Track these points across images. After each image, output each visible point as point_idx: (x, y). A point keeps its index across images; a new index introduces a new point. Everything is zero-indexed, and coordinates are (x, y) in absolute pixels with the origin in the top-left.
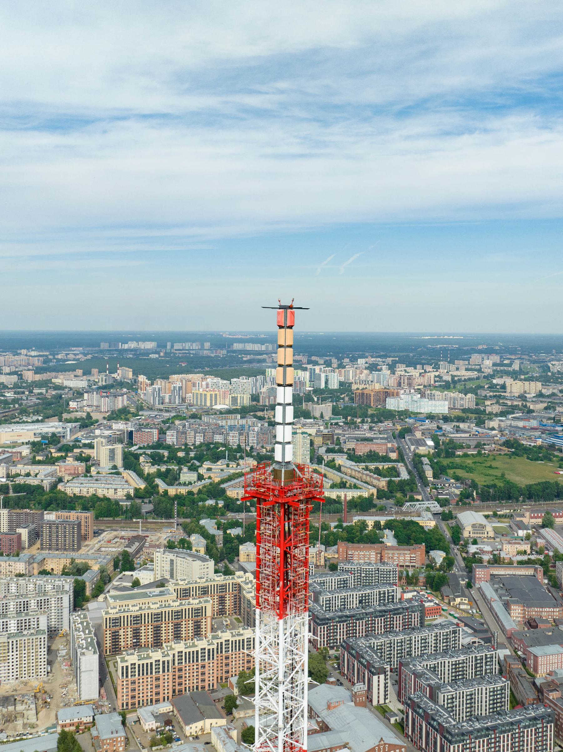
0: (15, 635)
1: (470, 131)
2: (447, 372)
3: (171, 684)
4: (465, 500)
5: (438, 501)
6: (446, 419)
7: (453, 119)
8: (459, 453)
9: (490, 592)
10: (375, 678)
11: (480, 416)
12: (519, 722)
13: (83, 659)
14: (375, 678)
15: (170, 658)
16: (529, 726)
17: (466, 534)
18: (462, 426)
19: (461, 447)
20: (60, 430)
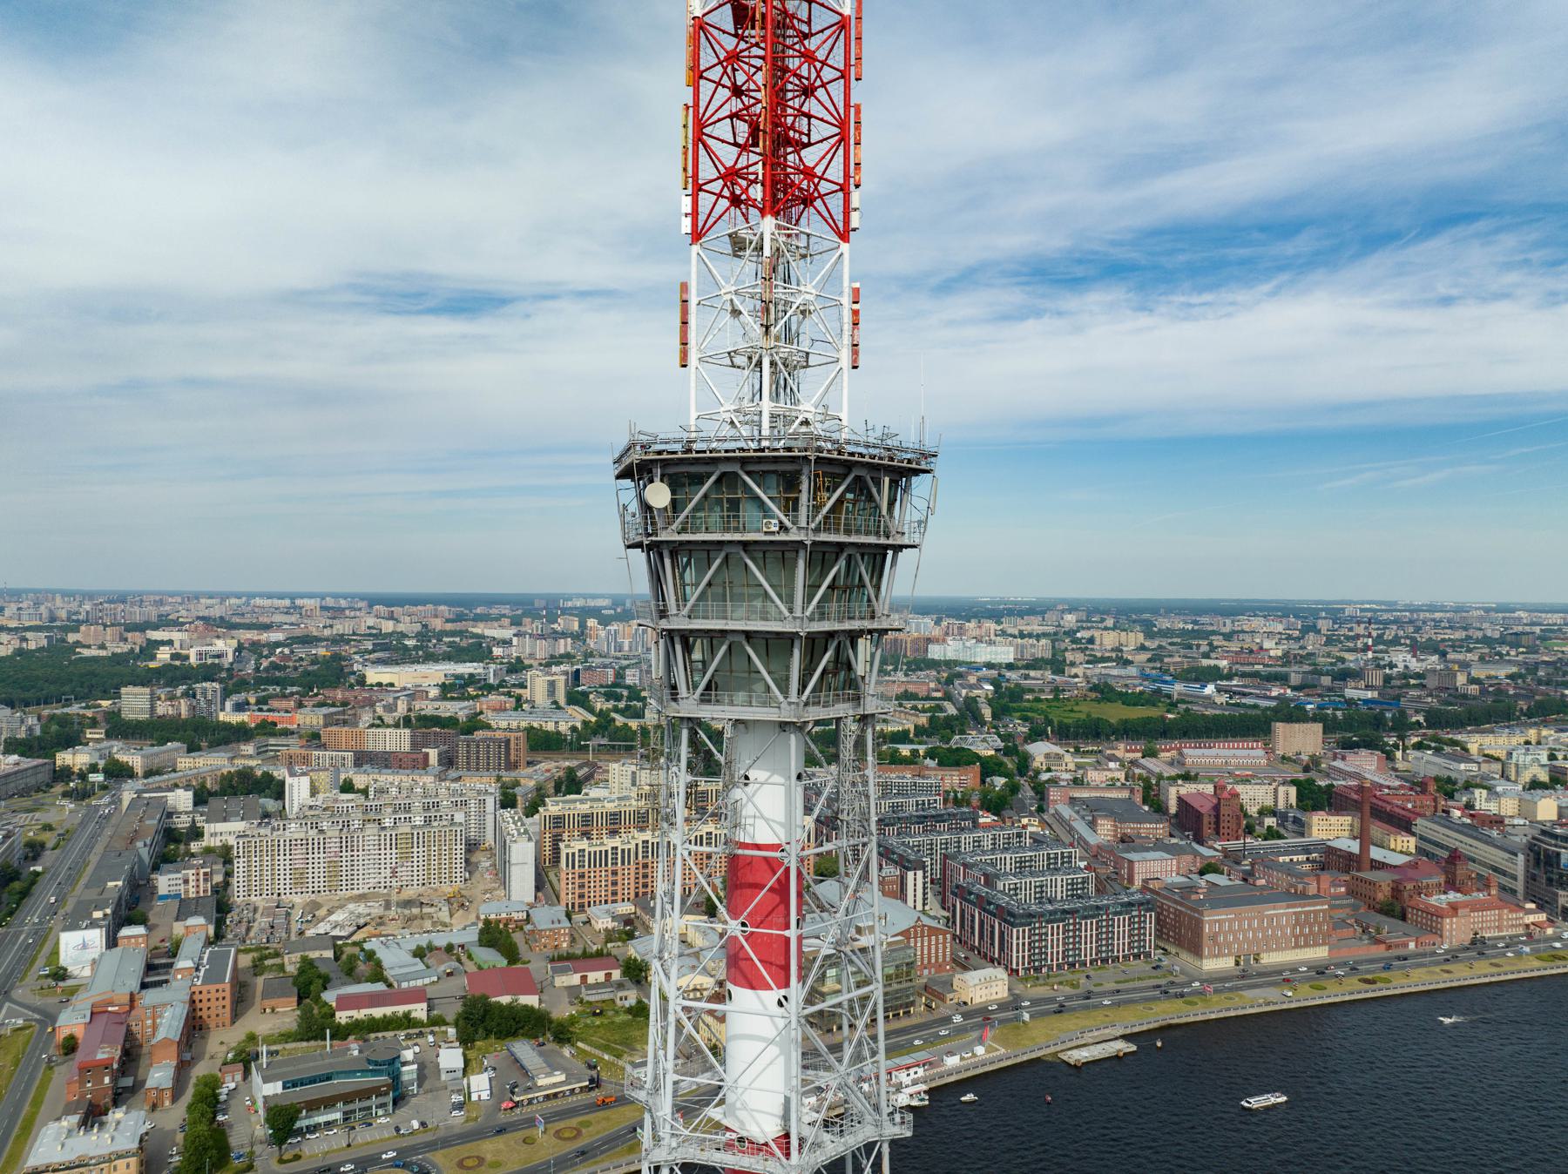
0: (420, 827)
1: (1038, 314)
2: (1010, 626)
3: (632, 886)
4: (1036, 735)
5: (1000, 736)
6: (1010, 667)
7: (1014, 297)
8: (1029, 697)
9: (1066, 812)
10: (910, 874)
11: (1057, 664)
12: (1107, 907)
13: (514, 846)
14: (910, 874)
15: (633, 847)
16: (1120, 913)
17: (1036, 764)
18: (1032, 673)
19: (1031, 691)
20: (480, 671)
